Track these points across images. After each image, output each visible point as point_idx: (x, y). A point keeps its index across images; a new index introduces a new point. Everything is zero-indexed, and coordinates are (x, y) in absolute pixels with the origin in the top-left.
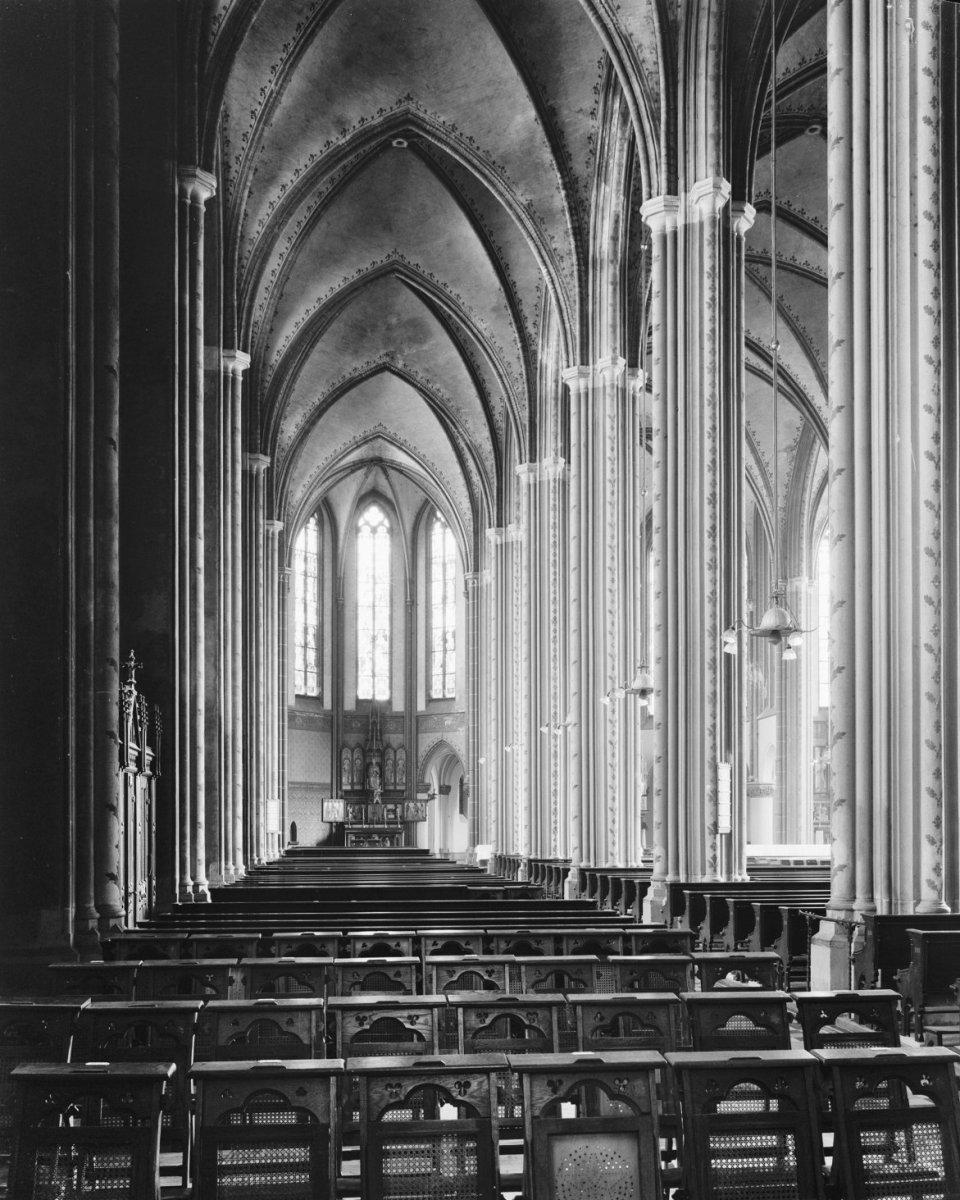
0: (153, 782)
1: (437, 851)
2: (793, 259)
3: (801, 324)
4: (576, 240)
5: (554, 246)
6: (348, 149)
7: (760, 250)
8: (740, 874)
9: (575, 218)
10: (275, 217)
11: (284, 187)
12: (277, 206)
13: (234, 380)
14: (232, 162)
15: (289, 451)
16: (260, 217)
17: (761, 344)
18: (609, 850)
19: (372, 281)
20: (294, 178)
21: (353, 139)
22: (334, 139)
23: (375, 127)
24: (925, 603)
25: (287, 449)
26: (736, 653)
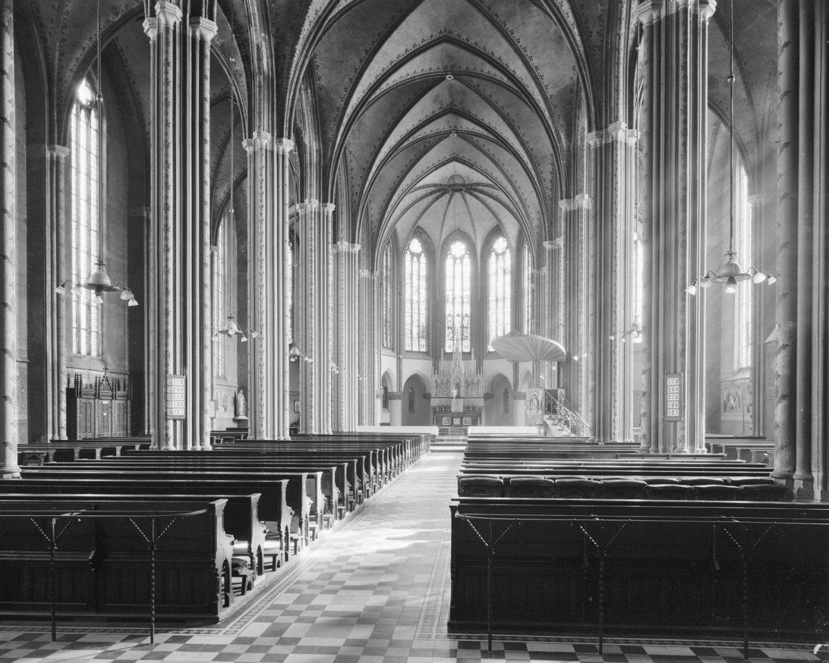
0: (146, 431)
1: (783, 252)
2: (482, 70)
3: (506, 111)
4: (244, 64)
5: (236, 68)
6: (120, 23)
7: (465, 67)
8: (700, 447)
9: (243, 50)
10: (79, 66)
11: (84, 49)
12: (80, 60)
13: (283, 156)
14: (48, 36)
15: (221, 207)
16: (71, 67)
17: (470, 130)
18: (613, 418)
19: (220, 100)
20: (89, 43)
21: (123, 17)
22: (111, 18)
23: (135, 9)
24: (232, 606)
25: (219, 206)
26: (307, 473)
